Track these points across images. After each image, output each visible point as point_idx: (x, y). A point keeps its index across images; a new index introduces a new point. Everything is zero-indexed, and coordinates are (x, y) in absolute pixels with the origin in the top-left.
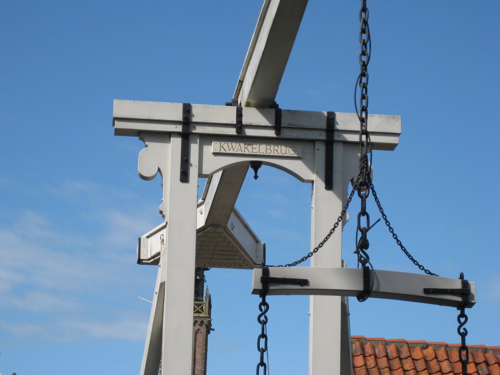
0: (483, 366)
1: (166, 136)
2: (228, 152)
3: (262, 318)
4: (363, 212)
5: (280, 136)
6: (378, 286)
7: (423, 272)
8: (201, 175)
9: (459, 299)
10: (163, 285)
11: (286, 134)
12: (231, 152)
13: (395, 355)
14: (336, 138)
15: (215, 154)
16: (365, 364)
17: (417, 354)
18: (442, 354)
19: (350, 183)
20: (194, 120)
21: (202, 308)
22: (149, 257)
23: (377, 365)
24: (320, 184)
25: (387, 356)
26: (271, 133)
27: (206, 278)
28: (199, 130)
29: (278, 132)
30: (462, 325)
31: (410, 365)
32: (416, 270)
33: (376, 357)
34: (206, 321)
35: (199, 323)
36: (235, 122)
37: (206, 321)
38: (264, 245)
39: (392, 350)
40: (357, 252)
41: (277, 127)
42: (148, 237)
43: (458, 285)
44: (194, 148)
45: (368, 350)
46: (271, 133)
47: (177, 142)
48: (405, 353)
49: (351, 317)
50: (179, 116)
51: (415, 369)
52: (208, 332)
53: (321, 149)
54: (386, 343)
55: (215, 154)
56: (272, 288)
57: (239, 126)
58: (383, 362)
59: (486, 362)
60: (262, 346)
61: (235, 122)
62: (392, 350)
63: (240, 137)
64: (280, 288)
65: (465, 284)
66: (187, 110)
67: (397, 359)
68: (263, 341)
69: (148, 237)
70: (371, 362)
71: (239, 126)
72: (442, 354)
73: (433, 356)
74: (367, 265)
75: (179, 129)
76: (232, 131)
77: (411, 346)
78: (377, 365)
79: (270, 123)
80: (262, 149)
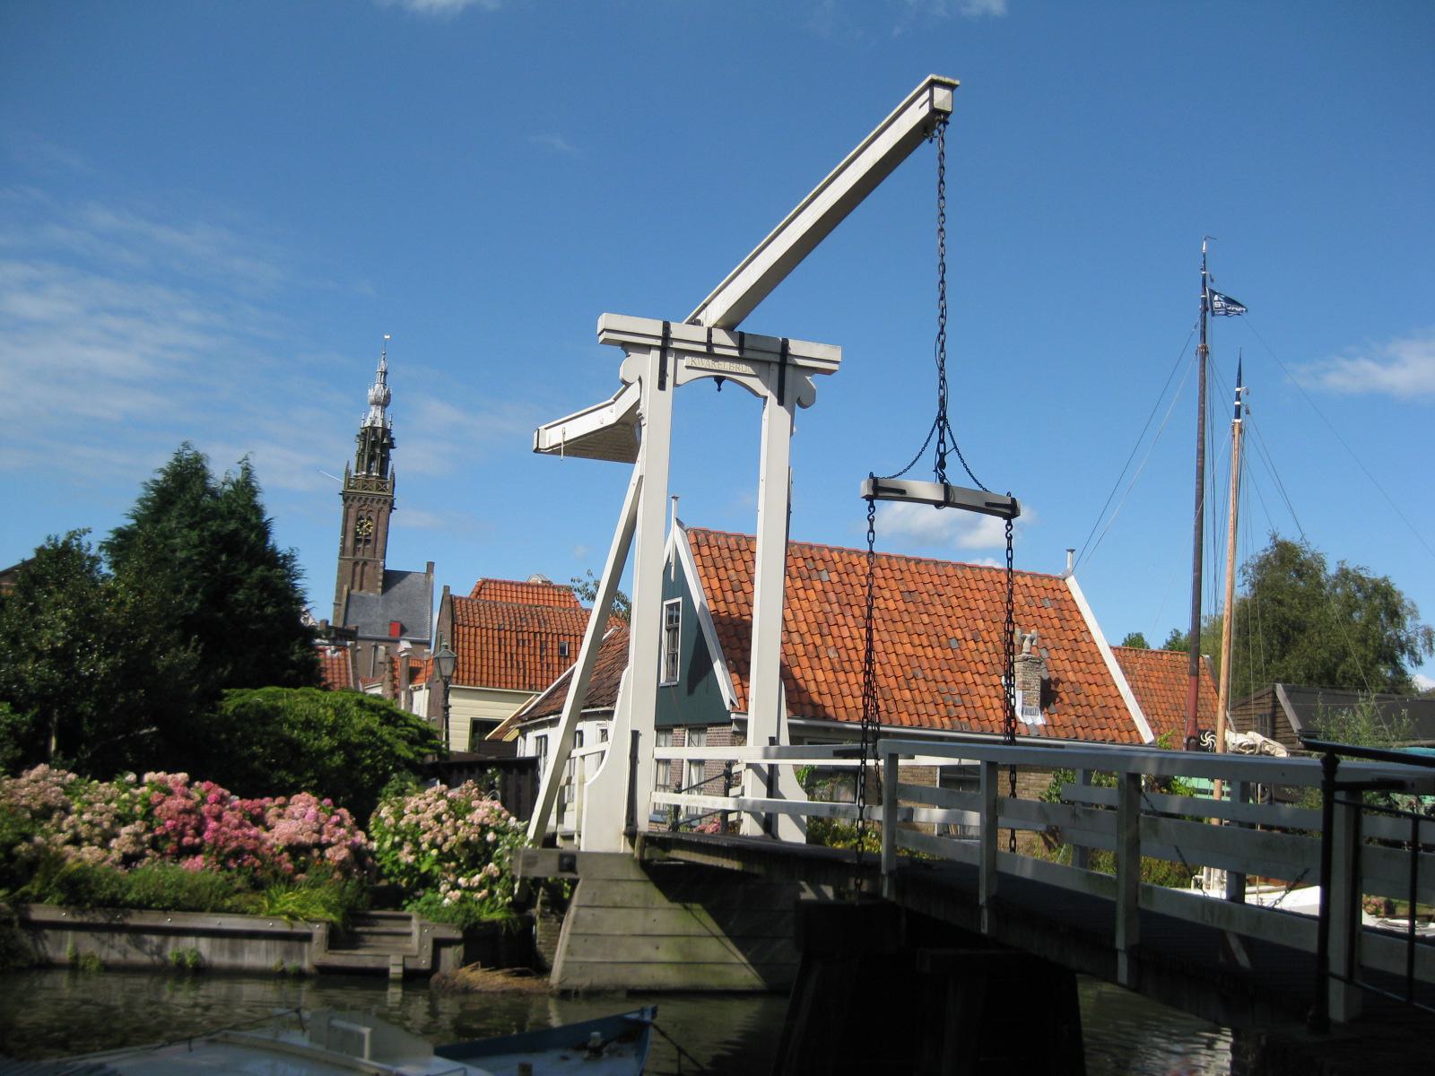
0: (810, 560)
1: (647, 348)
2: (698, 366)
3: (871, 517)
4: (942, 441)
6: (954, 499)
7: (981, 489)
8: (675, 385)
9: (1009, 512)
10: (641, 477)
11: (748, 354)
12: (701, 366)
13: (735, 547)
14: (789, 361)
15: (688, 367)
16: (711, 554)
17: (722, 542)
20: (672, 336)
21: (385, 487)
22: (547, 446)
24: (773, 400)
26: (736, 353)
27: (392, 457)
28: (676, 345)
29: (741, 353)
30: (1009, 531)
32: (976, 487)
35: (376, 500)
37: (389, 500)
39: (732, 542)
40: (936, 471)
41: (741, 348)
42: (546, 429)
43: (1009, 502)
44: (670, 360)
45: (713, 542)
46: (736, 353)
47: (656, 354)
50: (659, 332)
53: (775, 370)
54: (727, 536)
55: (688, 367)
56: (880, 494)
57: (709, 344)
58: (726, 553)
60: (871, 538)
61: (706, 341)
62: (732, 542)
63: (709, 354)
65: (1013, 500)
66: (666, 327)
68: (871, 534)
69: (546, 429)
70: (716, 552)
71: (709, 344)
74: (945, 481)
75: (659, 343)
76: (703, 349)
79: (735, 343)
80: (726, 366)
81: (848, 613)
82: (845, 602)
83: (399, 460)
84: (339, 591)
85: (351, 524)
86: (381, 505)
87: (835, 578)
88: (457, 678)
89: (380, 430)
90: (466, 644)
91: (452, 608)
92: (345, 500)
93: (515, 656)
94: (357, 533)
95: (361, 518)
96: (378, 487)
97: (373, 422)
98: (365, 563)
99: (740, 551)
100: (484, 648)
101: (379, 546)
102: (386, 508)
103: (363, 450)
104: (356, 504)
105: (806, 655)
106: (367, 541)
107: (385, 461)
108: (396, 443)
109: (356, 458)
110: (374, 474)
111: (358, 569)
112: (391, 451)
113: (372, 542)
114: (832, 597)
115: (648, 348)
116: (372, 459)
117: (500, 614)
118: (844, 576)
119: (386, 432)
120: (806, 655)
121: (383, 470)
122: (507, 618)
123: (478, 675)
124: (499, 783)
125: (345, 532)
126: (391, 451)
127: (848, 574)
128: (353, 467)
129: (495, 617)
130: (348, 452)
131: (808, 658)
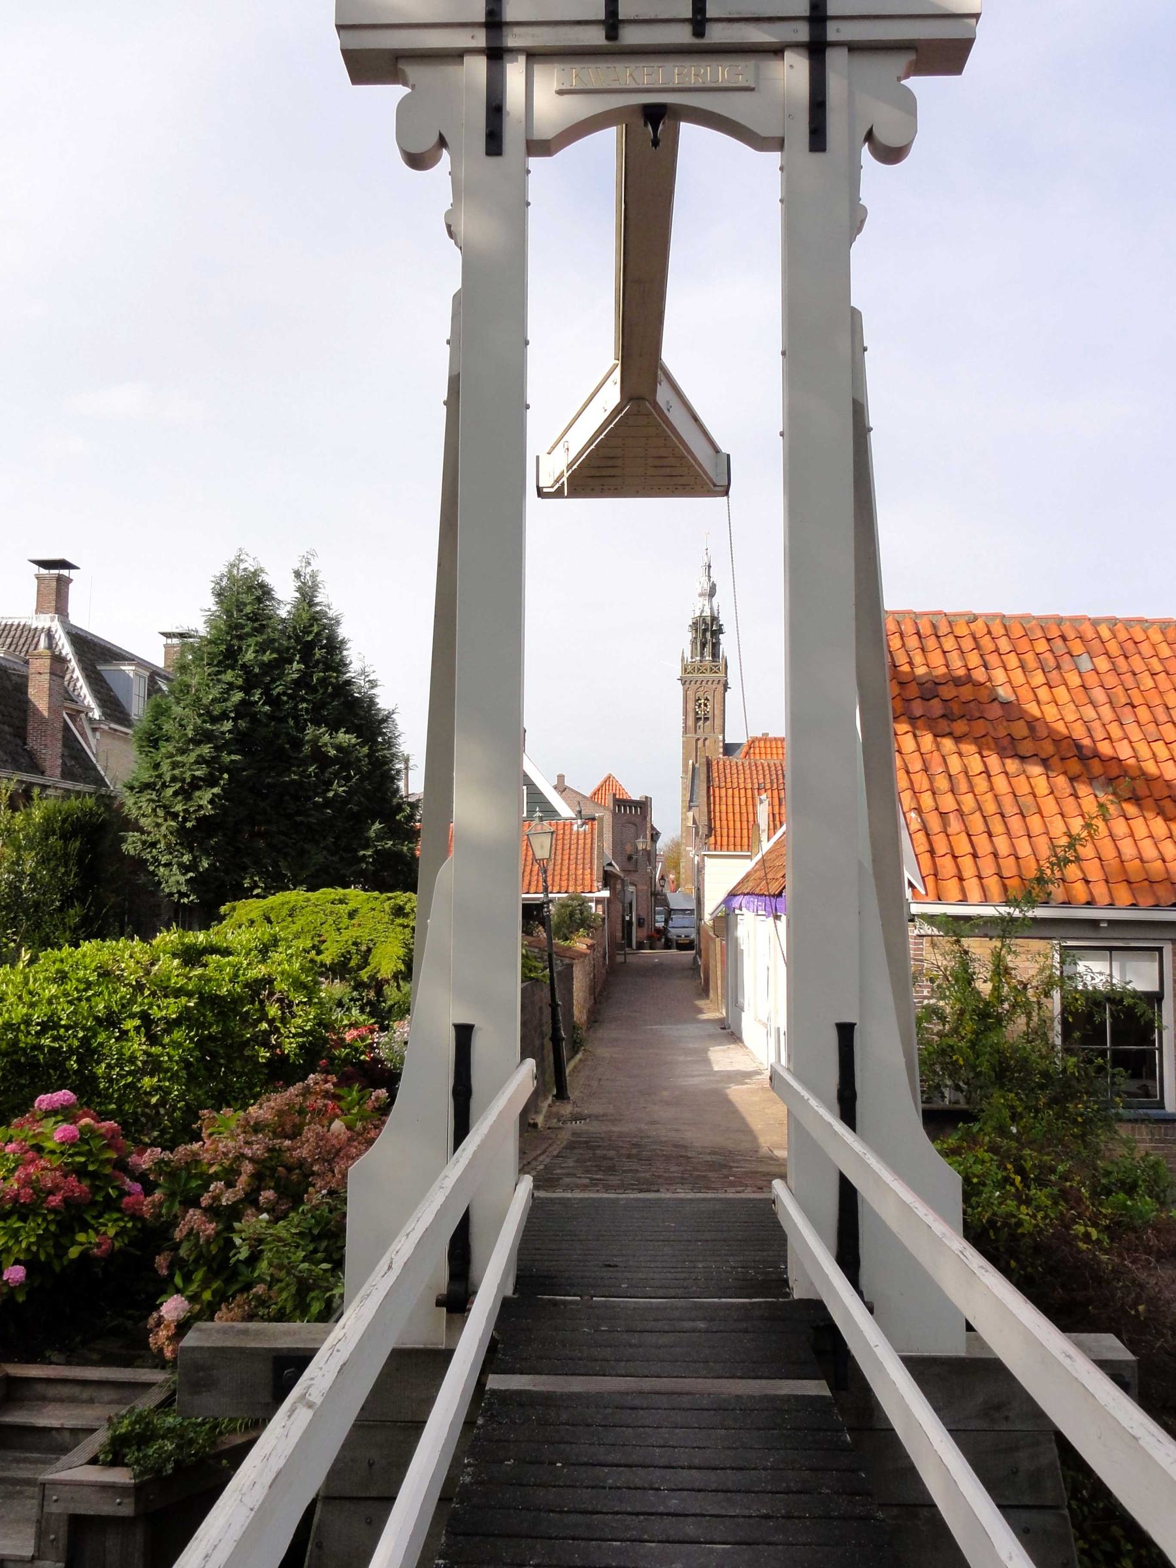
0: (1059, 642)
5: (705, 41)
14: (832, 35)
18: (998, 630)
19: (865, 149)
23: (903, 645)
25: (918, 633)
27: (722, 641)
29: (699, 32)
31: (951, 644)
33: (902, 635)
34: (722, 682)
36: (602, 16)
38: (728, 456)
47: (478, 67)
48: (943, 629)
49: (874, 437)
51: (960, 649)
52: (725, 690)
54: (916, 616)
59: (1064, 638)
64: (633, 95)
67: (933, 637)
72: (998, 630)
73: (985, 631)
77: (951, 620)
78: (903, 645)
81: (1128, 718)
82: (1124, 700)
83: (727, 643)
84: (685, 765)
85: (691, 705)
86: (714, 686)
87: (1103, 664)
88: (716, 843)
89: (709, 618)
90: (724, 807)
91: (708, 772)
92: (684, 684)
93: (777, 816)
94: (697, 713)
95: (699, 699)
96: (711, 669)
97: (702, 611)
98: (706, 739)
99: (938, 637)
100: (744, 810)
101: (718, 722)
102: (720, 688)
103: (695, 638)
104: (693, 687)
105: (1052, 792)
106: (706, 719)
107: (716, 646)
108: (725, 628)
109: (690, 646)
110: (707, 658)
111: (700, 743)
112: (721, 636)
113: (711, 719)
114: (1099, 695)
115: (457, 55)
116: (703, 645)
117: (761, 772)
118: (1121, 661)
119: (714, 619)
120: (1052, 792)
121: (715, 655)
122: (768, 776)
123: (738, 840)
124: (72, 1261)
125: (686, 713)
126: (721, 636)
127: (1126, 658)
128: (688, 654)
129: (755, 776)
130: (684, 640)
131: (1056, 798)
